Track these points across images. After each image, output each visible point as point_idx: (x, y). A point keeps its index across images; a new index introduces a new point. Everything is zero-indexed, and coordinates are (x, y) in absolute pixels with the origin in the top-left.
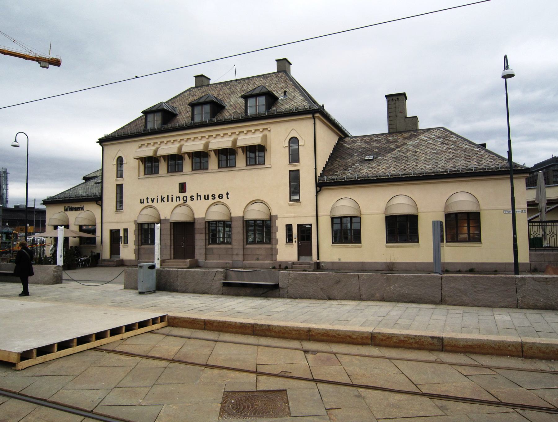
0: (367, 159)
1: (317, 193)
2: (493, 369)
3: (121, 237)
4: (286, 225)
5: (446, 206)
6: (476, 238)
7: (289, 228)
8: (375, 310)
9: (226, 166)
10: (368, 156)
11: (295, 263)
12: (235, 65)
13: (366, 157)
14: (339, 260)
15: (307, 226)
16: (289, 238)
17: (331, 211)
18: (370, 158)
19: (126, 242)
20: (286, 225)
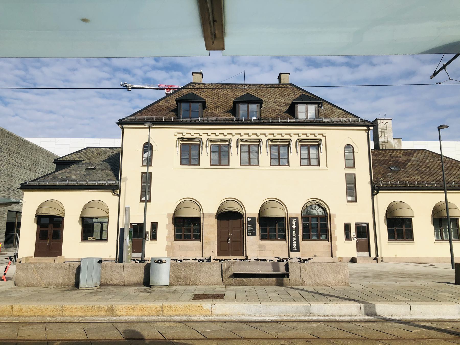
0: (90, 167)
1: (373, 195)
2: (316, 337)
3: (148, 232)
4: (157, 223)
5: (177, 210)
6: (392, 237)
7: (347, 226)
8: (404, 298)
9: (302, 165)
10: (91, 166)
11: (384, 260)
12: (244, 70)
13: (90, 166)
14: (396, 255)
15: (363, 225)
16: (348, 236)
17: (176, 211)
18: (92, 167)
19: (154, 237)
20: (157, 223)
